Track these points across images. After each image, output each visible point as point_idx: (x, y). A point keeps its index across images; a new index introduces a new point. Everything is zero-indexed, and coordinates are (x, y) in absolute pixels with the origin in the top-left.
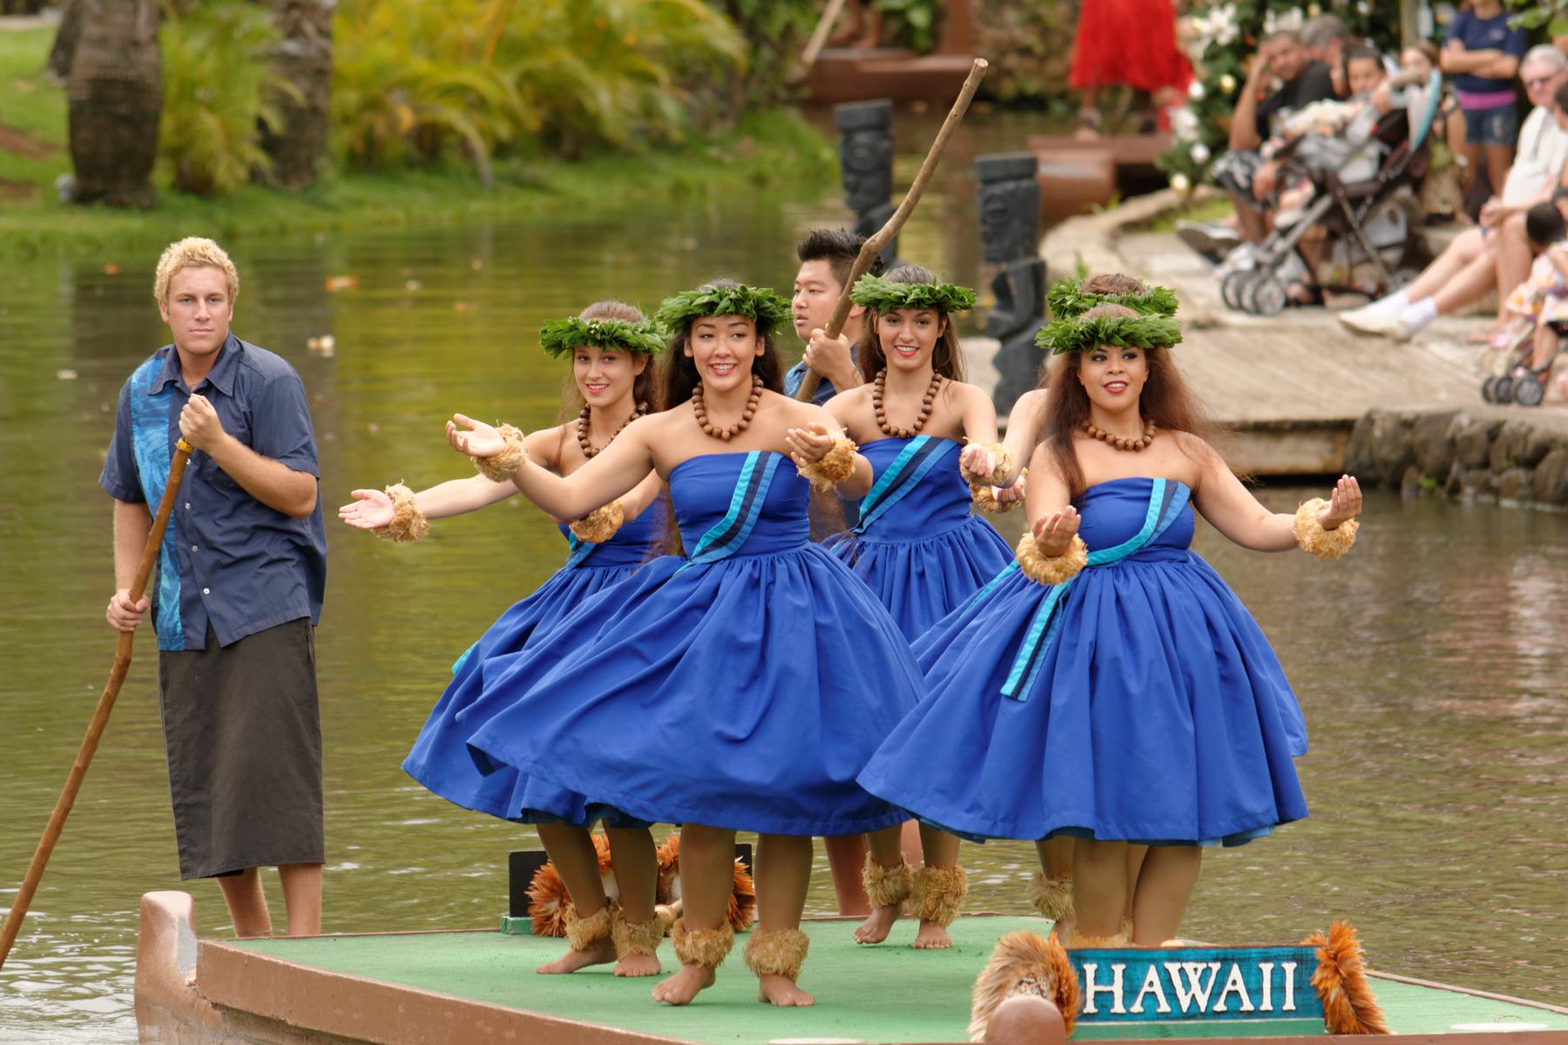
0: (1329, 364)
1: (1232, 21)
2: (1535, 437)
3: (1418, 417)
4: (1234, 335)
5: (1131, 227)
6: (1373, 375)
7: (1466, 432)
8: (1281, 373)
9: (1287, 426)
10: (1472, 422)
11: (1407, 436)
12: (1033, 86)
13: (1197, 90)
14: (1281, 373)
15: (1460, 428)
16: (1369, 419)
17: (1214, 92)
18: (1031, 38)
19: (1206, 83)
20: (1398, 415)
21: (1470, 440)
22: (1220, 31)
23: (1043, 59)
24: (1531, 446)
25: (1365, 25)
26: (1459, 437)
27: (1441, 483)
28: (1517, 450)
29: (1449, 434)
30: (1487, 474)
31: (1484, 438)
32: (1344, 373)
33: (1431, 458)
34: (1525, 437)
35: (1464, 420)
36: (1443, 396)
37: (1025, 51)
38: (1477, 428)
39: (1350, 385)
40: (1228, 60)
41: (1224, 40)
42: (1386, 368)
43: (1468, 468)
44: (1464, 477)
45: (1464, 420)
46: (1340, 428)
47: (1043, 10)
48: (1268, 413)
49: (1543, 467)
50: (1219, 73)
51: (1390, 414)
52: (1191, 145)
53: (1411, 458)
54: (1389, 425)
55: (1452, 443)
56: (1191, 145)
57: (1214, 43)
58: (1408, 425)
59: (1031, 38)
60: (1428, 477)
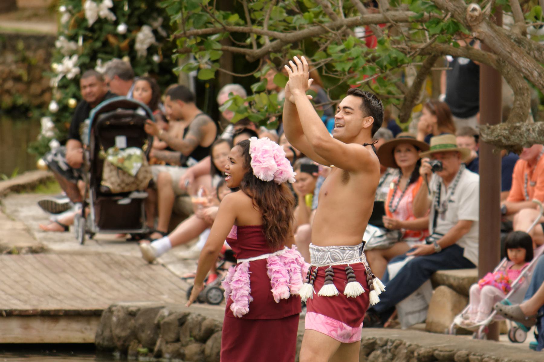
0: (104, 276)
1: (75, 66)
2: (206, 323)
3: (139, 310)
4: (53, 256)
5: (18, 189)
6: (127, 283)
7: (166, 320)
8: (72, 280)
9: (16, 313)
10: (170, 314)
11: (132, 323)
12: (21, 101)
13: (53, 106)
14: (72, 280)
15: (163, 317)
16: (110, 311)
17: (64, 108)
18: (22, 72)
19: (59, 102)
20: (127, 308)
21: (168, 324)
22: (68, 71)
23: (29, 83)
24: (203, 328)
25: (156, 69)
26: (162, 322)
27: (151, 350)
28: (196, 332)
29: (156, 321)
30: (177, 345)
31: (177, 323)
32: (111, 282)
33: (145, 335)
34: (200, 323)
35: (165, 312)
36: (165, 297)
37: (18, 79)
38: (172, 317)
39: (112, 289)
40: (72, 89)
41: (70, 76)
42: (138, 279)
43: (167, 343)
44: (164, 348)
45: (165, 312)
46: (96, 314)
47: (29, 54)
48: (52, 305)
49: (210, 343)
50: (67, 97)
51: (122, 307)
52: (49, 140)
53: (134, 335)
54: (122, 314)
55: (158, 326)
56: (49, 140)
57: (64, 77)
58: (132, 314)
59: (22, 72)
60: (144, 347)
